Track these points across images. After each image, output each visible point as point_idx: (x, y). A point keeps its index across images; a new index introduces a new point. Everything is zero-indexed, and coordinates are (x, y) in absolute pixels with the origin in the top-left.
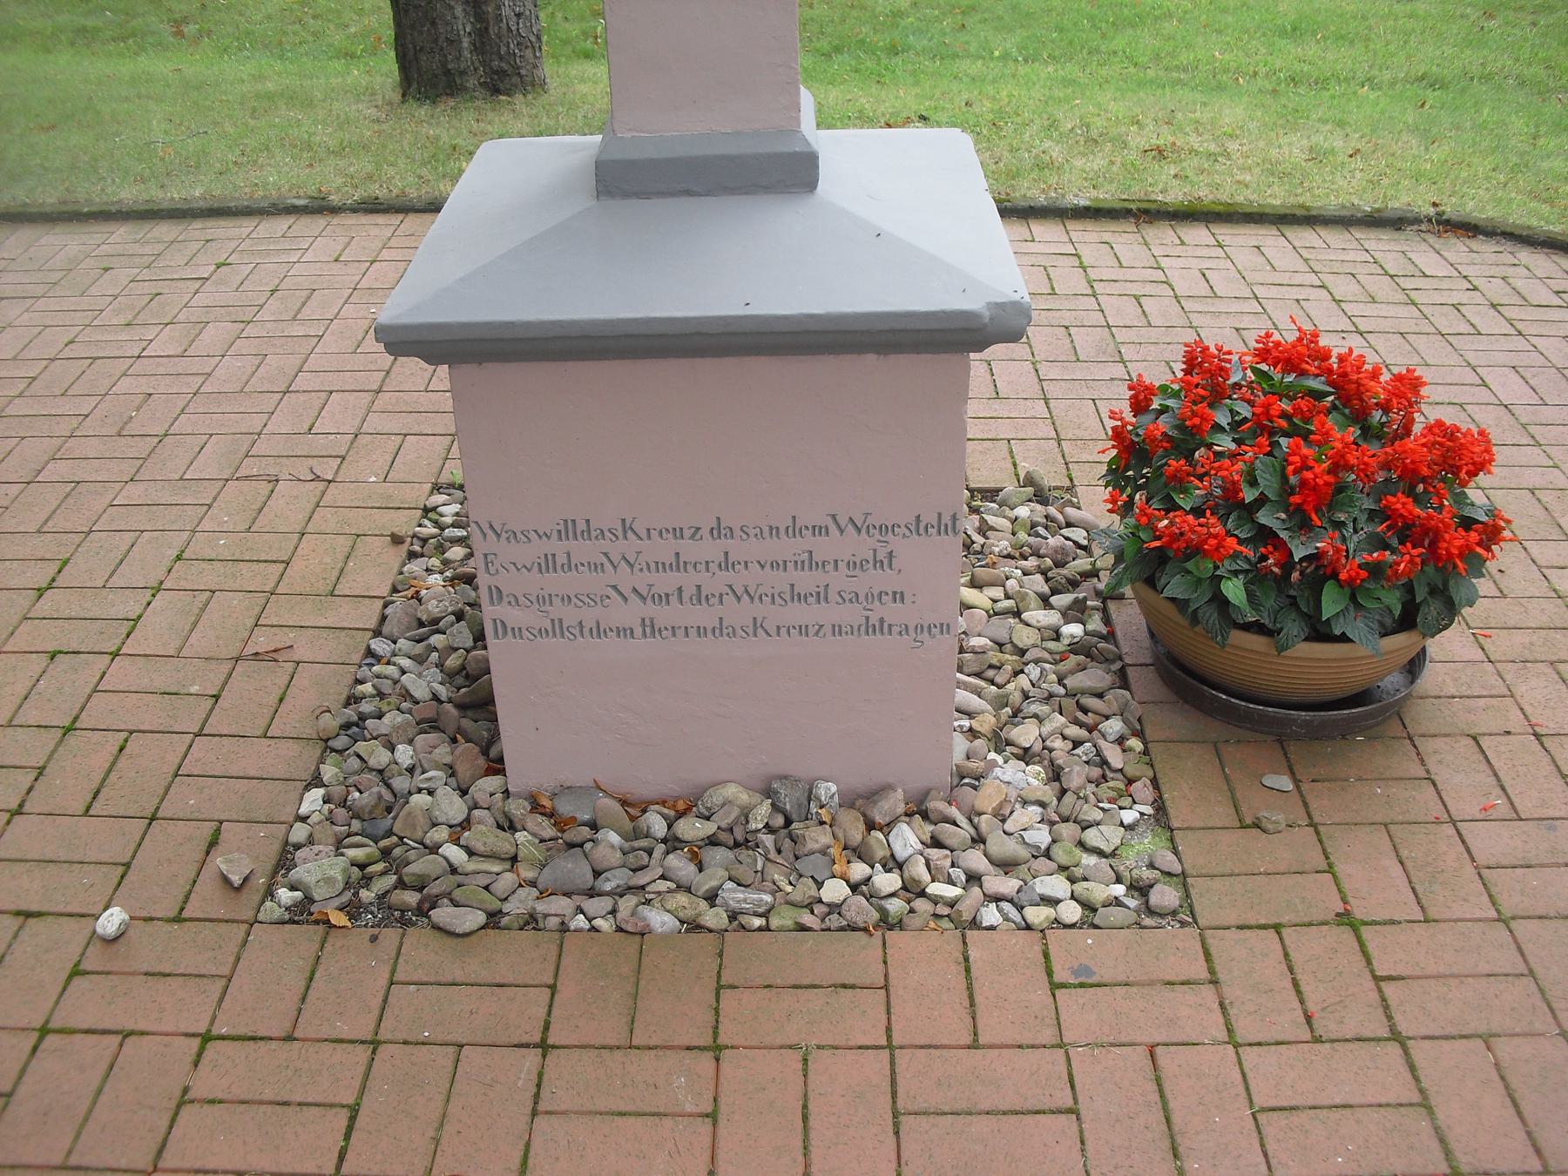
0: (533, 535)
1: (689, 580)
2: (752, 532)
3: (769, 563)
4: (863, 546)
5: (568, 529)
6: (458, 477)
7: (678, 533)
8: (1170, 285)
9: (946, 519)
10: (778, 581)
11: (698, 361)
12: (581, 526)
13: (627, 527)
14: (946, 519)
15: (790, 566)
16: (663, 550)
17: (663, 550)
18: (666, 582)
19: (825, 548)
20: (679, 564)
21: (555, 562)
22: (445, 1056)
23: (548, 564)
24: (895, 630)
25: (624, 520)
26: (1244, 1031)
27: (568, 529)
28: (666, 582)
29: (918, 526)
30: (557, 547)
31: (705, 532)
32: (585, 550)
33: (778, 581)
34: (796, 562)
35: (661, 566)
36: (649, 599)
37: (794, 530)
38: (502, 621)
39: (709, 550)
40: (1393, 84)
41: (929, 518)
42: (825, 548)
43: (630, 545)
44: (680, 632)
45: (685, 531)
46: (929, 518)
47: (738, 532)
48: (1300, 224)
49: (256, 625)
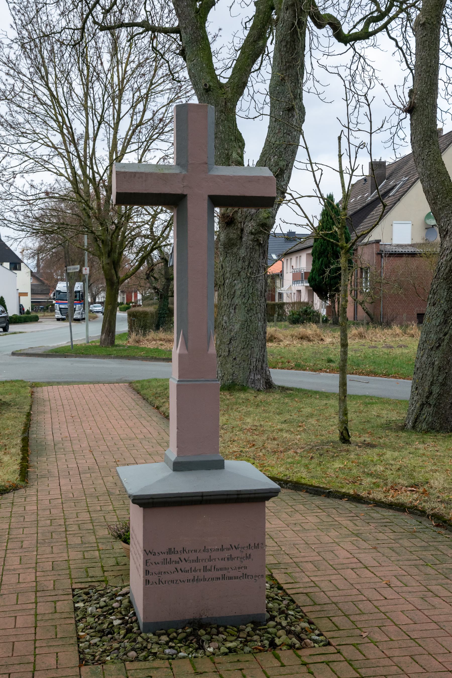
5: (170, 551)
6: (30, 245)
7: (195, 551)
9: (256, 545)
12: (173, 550)
13: (184, 550)
14: (256, 545)
16: (193, 556)
22: (20, 581)
26: (73, 577)
27: (170, 551)
30: (168, 557)
31: (202, 551)
32: (175, 557)
35: (193, 561)
39: (203, 555)
40: (61, 51)
43: (183, 556)
47: (157, 554)
48: (296, 388)
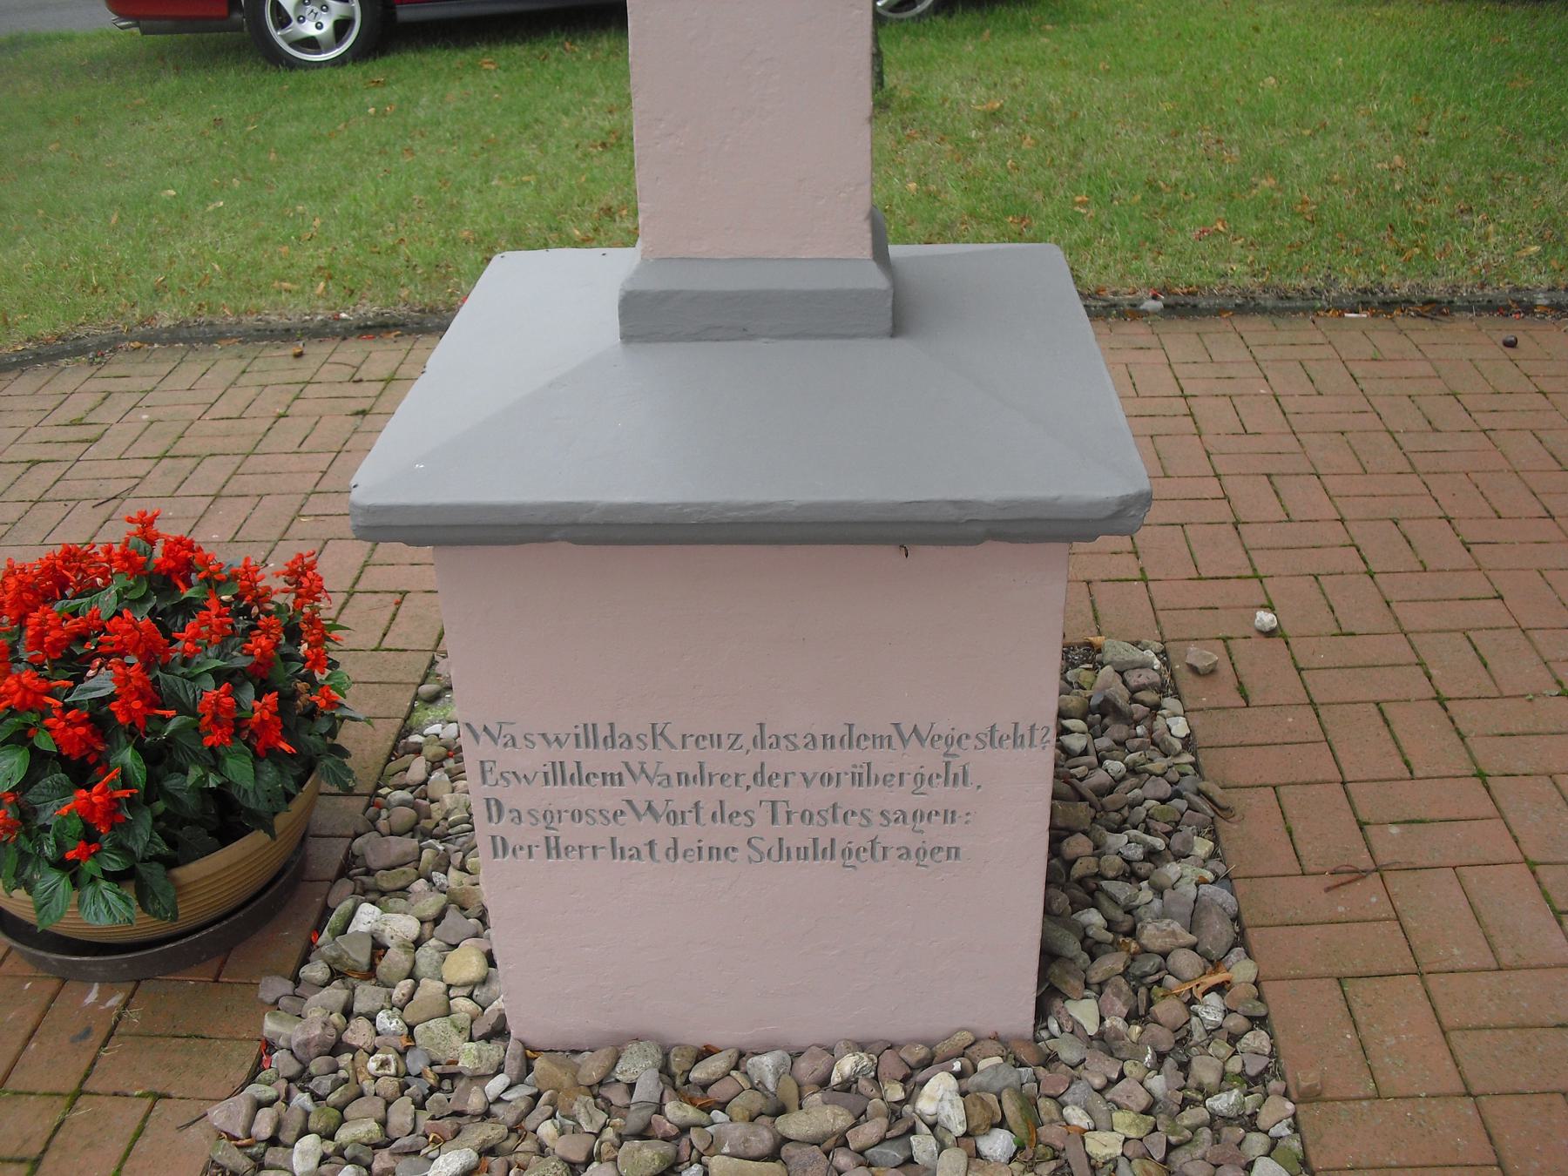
0: (539, 740)
1: (709, 796)
2: (800, 742)
3: (819, 776)
4: (931, 760)
5: (589, 736)
8: (329, 540)
10: (820, 796)
11: (625, 547)
12: (603, 731)
15: (845, 780)
17: (686, 760)
18: (683, 797)
19: (717, 761)
20: (703, 777)
21: (563, 772)
23: (556, 774)
24: (892, 853)
25: (653, 725)
27: (589, 736)
28: (683, 797)
29: (992, 738)
33: (820, 796)
34: (853, 773)
35: (683, 778)
36: (664, 818)
37: (852, 739)
38: (503, 839)
39: (746, 762)
41: (1005, 728)
42: (884, 761)
44: (588, 852)
45: (724, 738)
46: (1005, 728)
47: (520, 741)
49: (1454, 868)
